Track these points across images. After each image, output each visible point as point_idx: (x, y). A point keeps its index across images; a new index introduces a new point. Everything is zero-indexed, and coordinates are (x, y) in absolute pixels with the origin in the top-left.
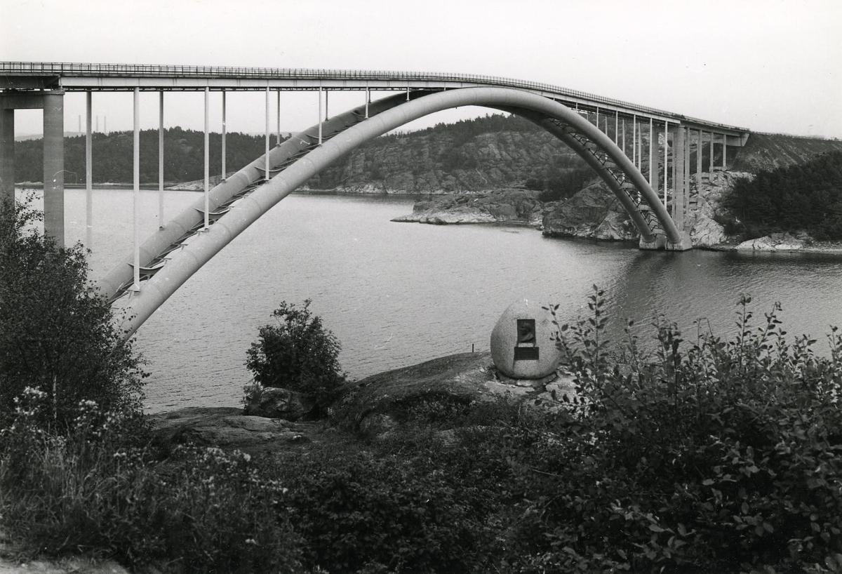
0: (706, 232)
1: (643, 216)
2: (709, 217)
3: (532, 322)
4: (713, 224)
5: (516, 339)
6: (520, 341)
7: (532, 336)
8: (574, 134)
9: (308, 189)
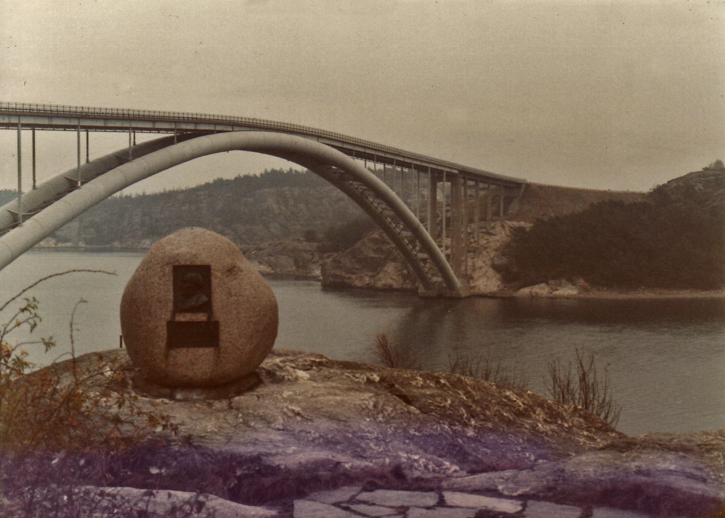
0: (484, 279)
1: (422, 264)
2: (486, 265)
3: (206, 270)
4: (491, 272)
5: (170, 306)
6: (177, 310)
7: (204, 298)
8: (351, 182)
9: (83, 245)
